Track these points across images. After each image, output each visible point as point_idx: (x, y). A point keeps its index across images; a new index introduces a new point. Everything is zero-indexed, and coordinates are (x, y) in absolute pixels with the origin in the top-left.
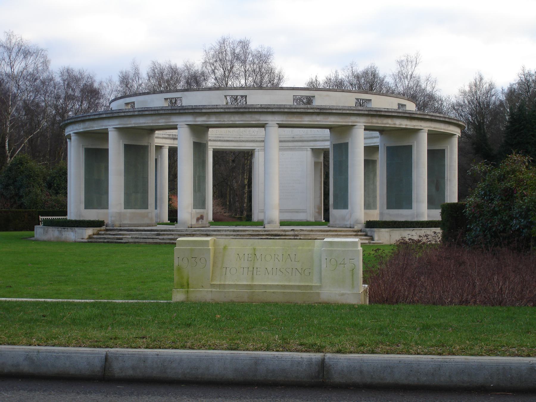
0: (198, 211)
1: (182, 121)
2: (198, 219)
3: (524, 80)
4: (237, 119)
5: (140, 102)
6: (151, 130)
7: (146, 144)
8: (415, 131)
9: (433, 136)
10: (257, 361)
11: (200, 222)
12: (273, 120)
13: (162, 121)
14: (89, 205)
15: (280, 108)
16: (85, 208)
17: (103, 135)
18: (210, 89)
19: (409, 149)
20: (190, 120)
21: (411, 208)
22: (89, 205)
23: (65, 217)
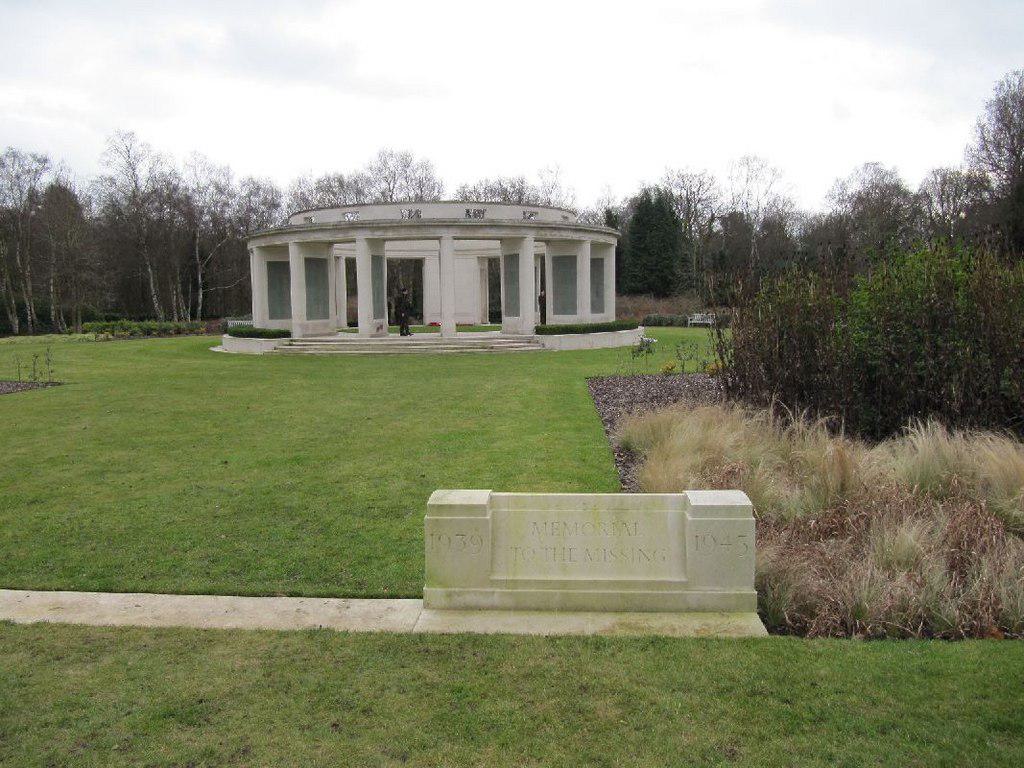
0: (378, 321)
1: (361, 236)
2: (378, 329)
4: (414, 233)
5: (317, 218)
6: (331, 244)
8: (580, 242)
9: (595, 246)
10: (240, 325)
11: (380, 331)
12: (447, 234)
13: (340, 236)
14: (273, 316)
17: (285, 249)
20: (368, 234)
22: (273, 316)
23: (247, 323)
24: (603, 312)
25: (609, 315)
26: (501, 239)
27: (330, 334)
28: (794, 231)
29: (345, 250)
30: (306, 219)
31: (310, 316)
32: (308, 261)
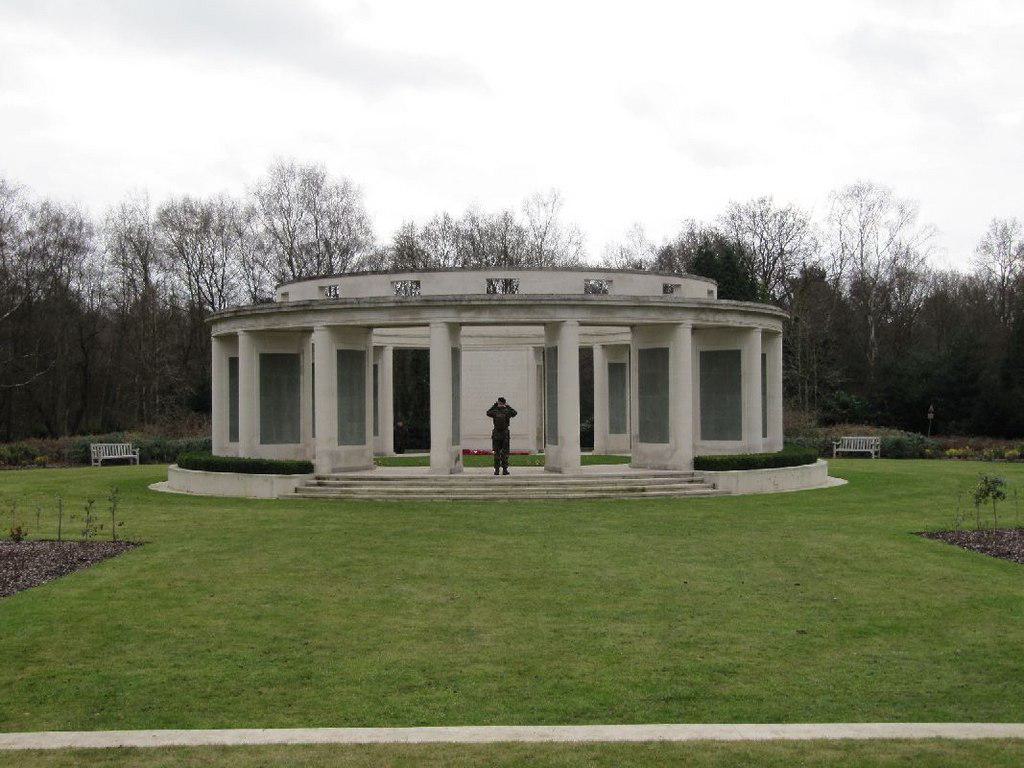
3: (183, 304)
6: (370, 328)
7: (363, 349)
8: (749, 330)
14: (267, 437)
15: (569, 300)
16: (262, 443)
18: (386, 272)
19: (736, 356)
20: (452, 316)
21: (740, 439)
24: (740, 439)
25: (776, 444)
26: (632, 326)
27: (366, 468)
28: (919, 293)
29: (415, 337)
30: (322, 288)
31: (343, 439)
32: (341, 354)
